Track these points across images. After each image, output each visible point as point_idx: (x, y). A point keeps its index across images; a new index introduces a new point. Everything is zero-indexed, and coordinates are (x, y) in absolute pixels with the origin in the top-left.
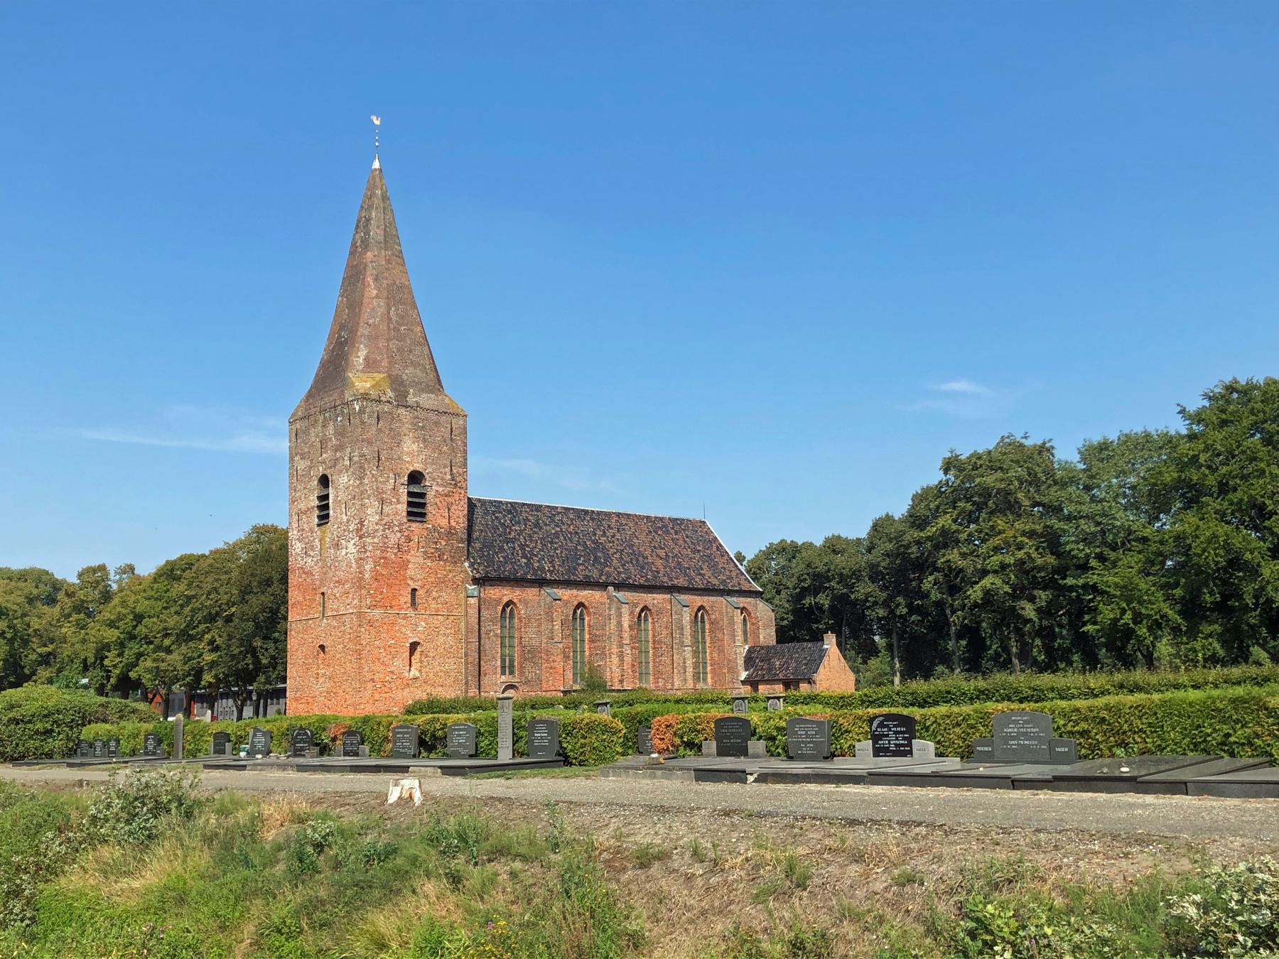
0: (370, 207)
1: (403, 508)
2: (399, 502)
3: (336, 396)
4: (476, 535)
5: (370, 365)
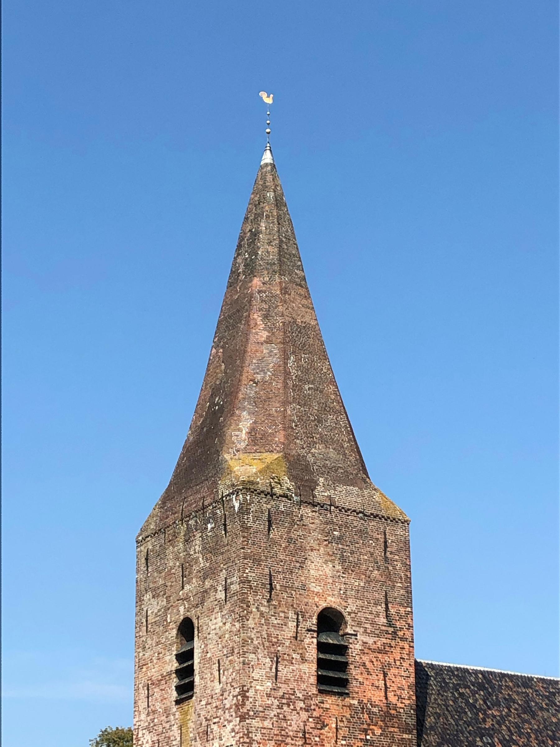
0: (258, 217)
1: (310, 669)
2: (303, 660)
3: (204, 491)
4: (430, 721)
5: (258, 440)
